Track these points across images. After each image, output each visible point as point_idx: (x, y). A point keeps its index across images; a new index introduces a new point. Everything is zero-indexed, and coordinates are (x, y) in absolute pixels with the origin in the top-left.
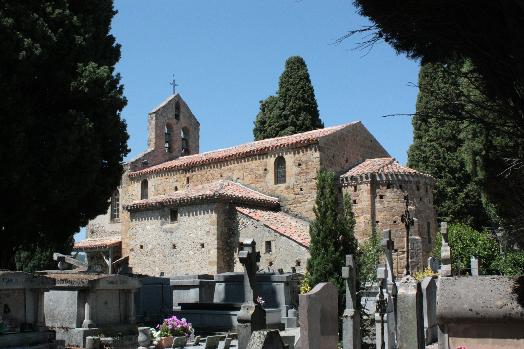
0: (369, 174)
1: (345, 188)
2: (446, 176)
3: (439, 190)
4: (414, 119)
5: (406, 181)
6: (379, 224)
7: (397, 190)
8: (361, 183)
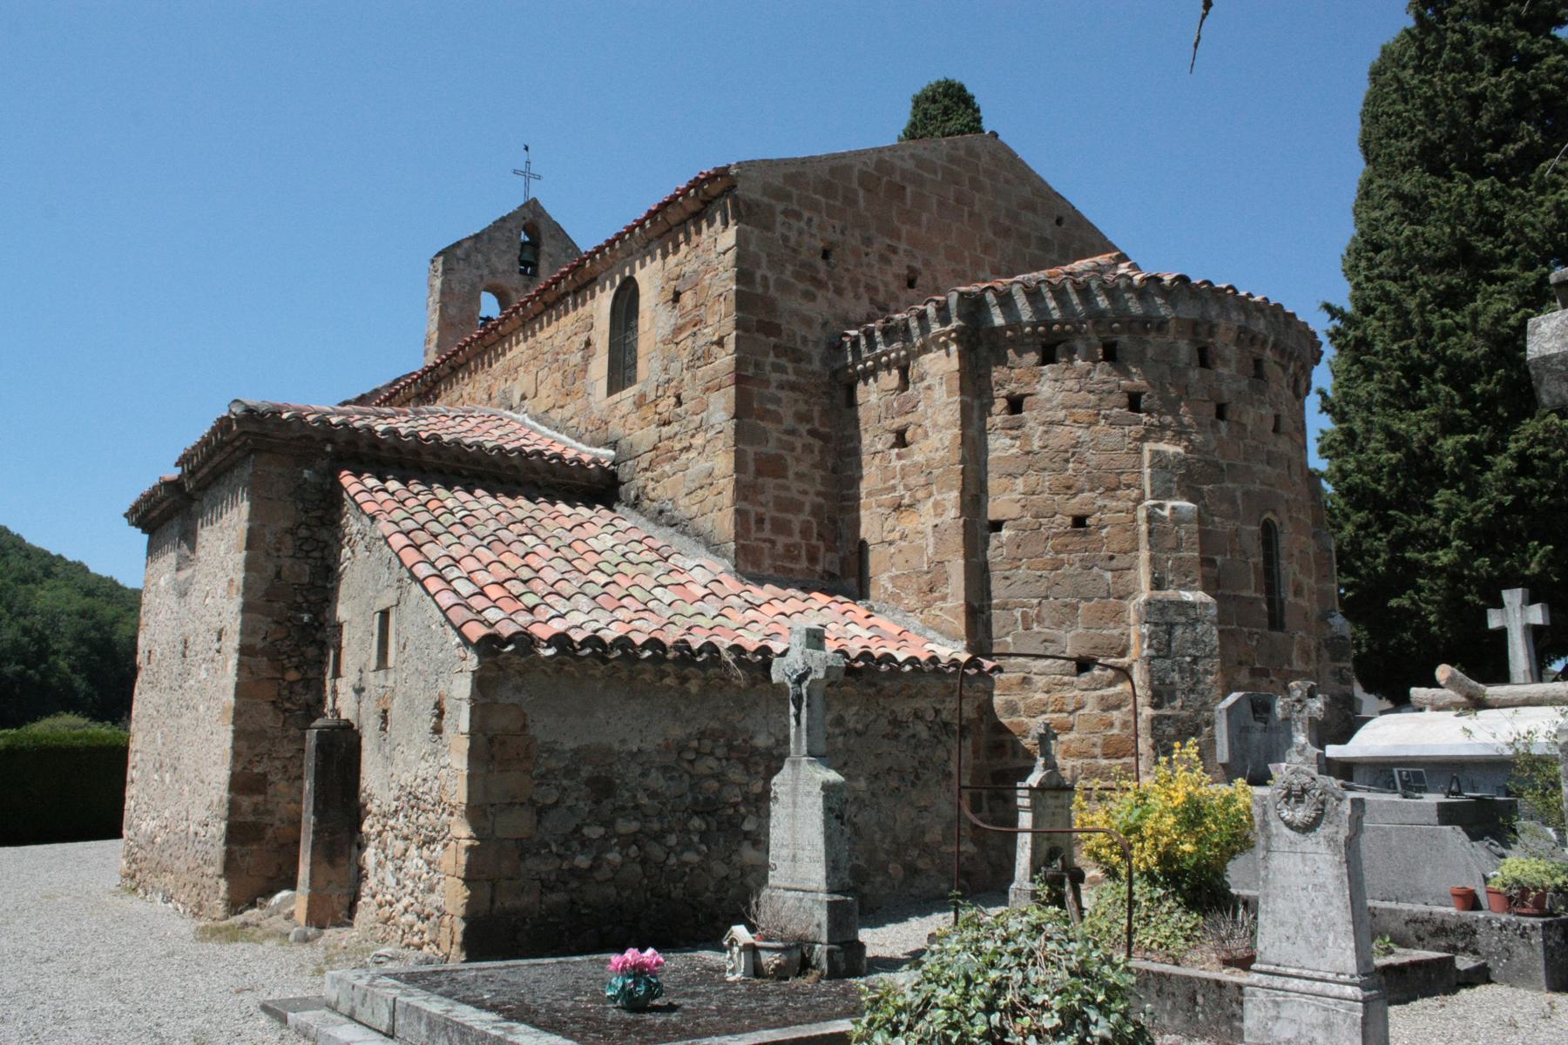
2: (1434, 398)
3: (1409, 449)
4: (1349, 254)
5: (1134, 319)
6: (1005, 533)
7: (1088, 365)
8: (925, 349)
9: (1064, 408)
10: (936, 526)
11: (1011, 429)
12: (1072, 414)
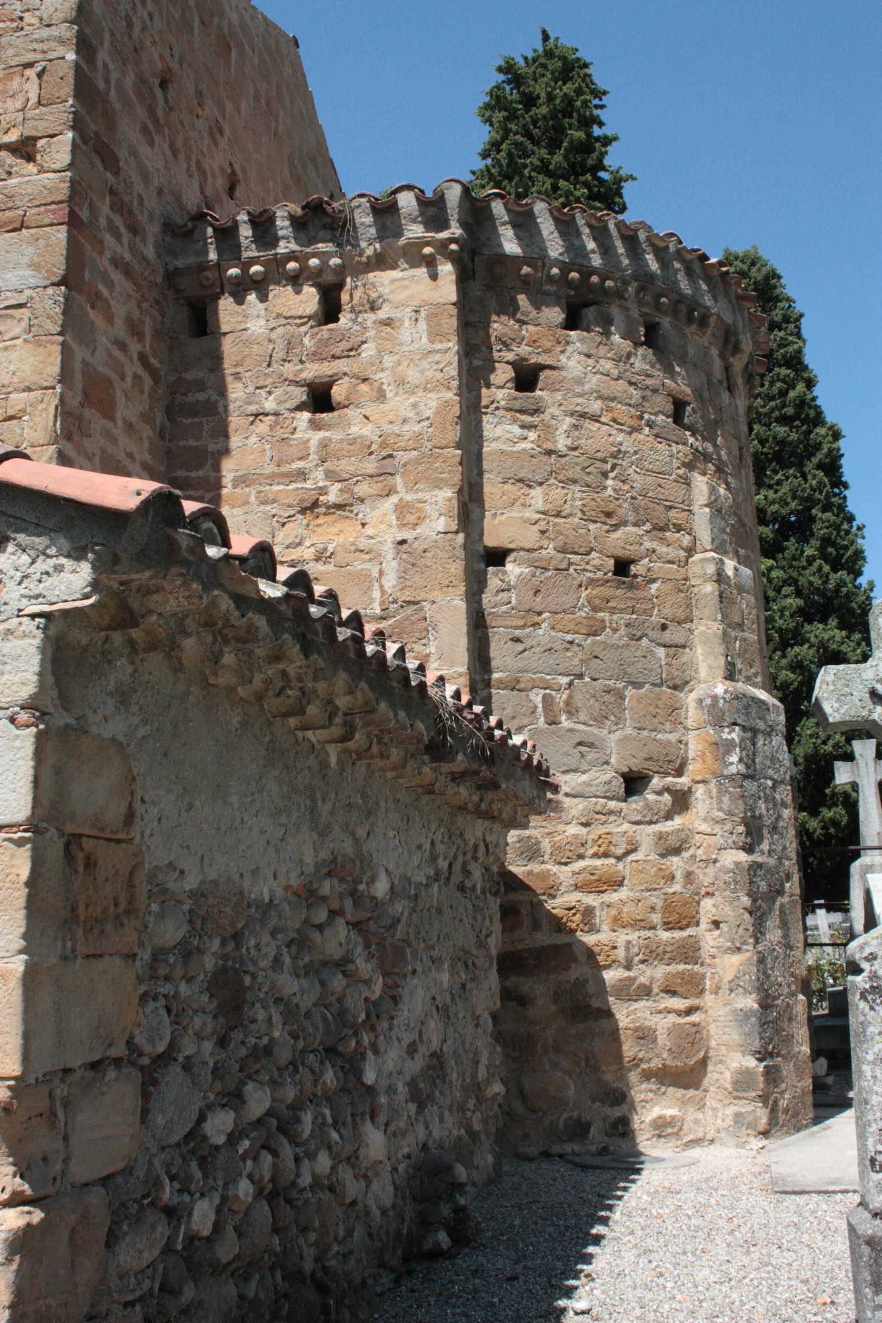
0: (454, 194)
1: (240, 301)
6: (513, 569)
7: (626, 345)
8: (381, 262)
9: (599, 397)
10: (403, 542)
11: (521, 412)
12: (610, 409)
